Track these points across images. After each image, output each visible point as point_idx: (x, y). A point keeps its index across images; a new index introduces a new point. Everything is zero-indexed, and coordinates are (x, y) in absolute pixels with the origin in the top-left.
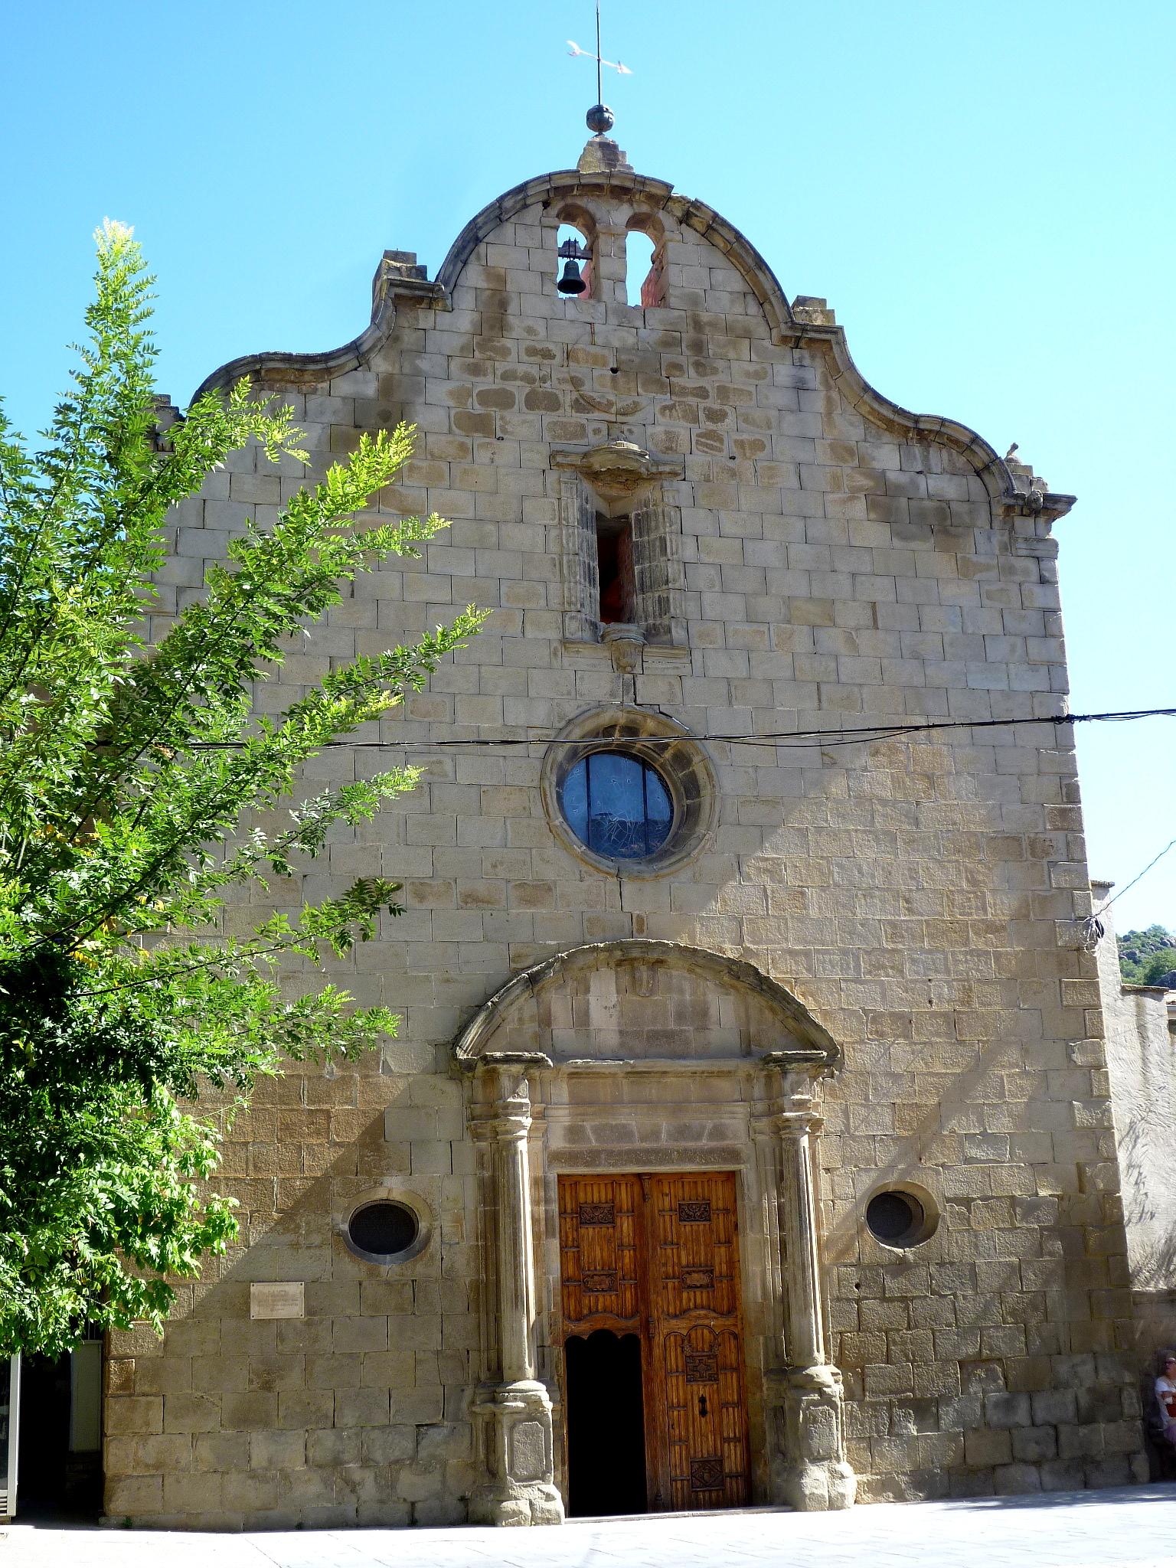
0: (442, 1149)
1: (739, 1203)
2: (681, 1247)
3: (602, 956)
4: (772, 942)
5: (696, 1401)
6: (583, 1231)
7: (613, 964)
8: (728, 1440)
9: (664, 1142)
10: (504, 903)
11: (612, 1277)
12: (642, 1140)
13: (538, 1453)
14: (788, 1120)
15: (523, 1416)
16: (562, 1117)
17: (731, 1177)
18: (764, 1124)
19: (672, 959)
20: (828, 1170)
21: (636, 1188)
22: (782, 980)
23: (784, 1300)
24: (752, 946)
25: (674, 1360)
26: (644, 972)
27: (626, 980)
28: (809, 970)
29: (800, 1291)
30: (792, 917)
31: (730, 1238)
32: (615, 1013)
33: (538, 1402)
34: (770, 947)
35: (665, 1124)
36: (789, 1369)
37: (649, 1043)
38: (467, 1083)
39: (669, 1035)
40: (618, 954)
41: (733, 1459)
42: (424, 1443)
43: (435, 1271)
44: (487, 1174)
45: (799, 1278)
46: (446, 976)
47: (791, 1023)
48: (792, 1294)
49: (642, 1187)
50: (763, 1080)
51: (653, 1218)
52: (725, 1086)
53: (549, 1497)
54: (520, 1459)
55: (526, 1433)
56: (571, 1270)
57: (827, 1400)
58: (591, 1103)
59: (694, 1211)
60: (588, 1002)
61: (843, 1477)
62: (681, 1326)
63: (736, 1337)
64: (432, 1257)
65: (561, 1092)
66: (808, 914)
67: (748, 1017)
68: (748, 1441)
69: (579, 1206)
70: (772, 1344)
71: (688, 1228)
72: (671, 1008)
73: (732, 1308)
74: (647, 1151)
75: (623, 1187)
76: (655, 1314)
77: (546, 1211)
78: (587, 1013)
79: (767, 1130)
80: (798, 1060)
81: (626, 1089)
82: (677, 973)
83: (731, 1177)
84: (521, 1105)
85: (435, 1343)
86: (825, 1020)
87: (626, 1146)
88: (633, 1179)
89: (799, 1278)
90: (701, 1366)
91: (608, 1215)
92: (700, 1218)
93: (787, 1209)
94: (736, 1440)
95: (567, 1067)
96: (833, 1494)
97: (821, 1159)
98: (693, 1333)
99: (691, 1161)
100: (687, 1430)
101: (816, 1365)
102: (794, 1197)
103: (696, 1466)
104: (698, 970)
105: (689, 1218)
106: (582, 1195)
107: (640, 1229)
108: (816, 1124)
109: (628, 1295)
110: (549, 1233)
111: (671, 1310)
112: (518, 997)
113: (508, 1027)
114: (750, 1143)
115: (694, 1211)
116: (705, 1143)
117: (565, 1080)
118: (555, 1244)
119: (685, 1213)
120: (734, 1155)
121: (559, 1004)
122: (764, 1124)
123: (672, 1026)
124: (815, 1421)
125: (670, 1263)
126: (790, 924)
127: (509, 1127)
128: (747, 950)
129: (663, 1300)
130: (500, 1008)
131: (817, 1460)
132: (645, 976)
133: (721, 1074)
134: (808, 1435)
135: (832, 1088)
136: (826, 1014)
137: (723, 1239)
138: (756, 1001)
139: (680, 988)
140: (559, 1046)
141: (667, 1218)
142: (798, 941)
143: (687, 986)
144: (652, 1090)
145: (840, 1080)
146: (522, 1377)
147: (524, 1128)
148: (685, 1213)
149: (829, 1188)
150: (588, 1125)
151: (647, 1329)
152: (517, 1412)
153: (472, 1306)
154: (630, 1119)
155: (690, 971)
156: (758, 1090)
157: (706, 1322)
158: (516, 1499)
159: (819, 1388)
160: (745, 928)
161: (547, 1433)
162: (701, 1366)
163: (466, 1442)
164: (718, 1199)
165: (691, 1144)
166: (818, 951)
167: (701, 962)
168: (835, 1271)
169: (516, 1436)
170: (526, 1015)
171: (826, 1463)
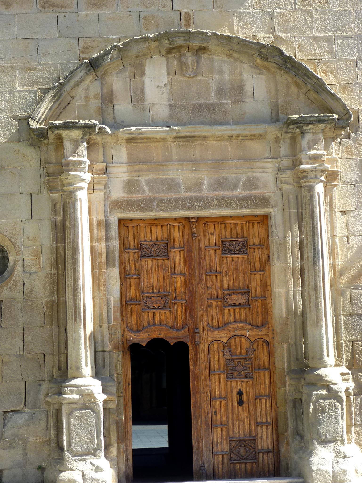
0: (24, 200)
1: (270, 239)
2: (225, 274)
3: (153, 45)
4: (299, 31)
5: (235, 394)
6: (143, 262)
7: (163, 52)
8: (261, 424)
9: (206, 191)
10: (75, 6)
11: (165, 299)
12: (188, 190)
13: (91, 435)
14: (304, 171)
15: (79, 406)
16: (121, 174)
17: (266, 218)
18: (288, 176)
19: (212, 46)
20: (344, 212)
21: (186, 229)
22: (308, 62)
23: (303, 314)
24: (281, 35)
25: (217, 361)
26: (189, 58)
27: (175, 65)
28: (331, 52)
29: (313, 308)
30: (316, 10)
31: (264, 268)
32: (166, 91)
33: (91, 395)
34: (297, 35)
35: (206, 178)
36: (305, 367)
37: (195, 113)
38: (44, 149)
39: (211, 108)
40: (166, 42)
41: (265, 439)
42: (9, 425)
43: (18, 294)
44: (59, 218)
45: (313, 297)
46: (27, 65)
47: (313, 95)
48: (308, 311)
49: (191, 227)
50: (288, 141)
51: (200, 252)
52: (257, 147)
53: (98, 469)
54: (76, 439)
55: (81, 419)
56: (133, 292)
57: (334, 395)
58: (146, 162)
59: (235, 246)
60: (143, 83)
61: (345, 456)
62: (223, 336)
63: (268, 344)
64: (15, 283)
65: (121, 154)
66: (330, 8)
67: (277, 91)
68: (276, 426)
69: (137, 243)
70: (293, 349)
71: (229, 260)
72: (213, 86)
73: (265, 321)
74: (191, 199)
75: (176, 229)
76: (201, 327)
77: (107, 247)
78: (142, 92)
79: (291, 181)
80: (312, 122)
81: (175, 150)
82: (218, 59)
83: (266, 218)
84: (80, 163)
85: (18, 348)
86: (344, 92)
87: (174, 195)
88: (184, 222)
89: (313, 297)
90: (239, 366)
91: (164, 250)
92: (240, 252)
93: (305, 242)
94: (268, 424)
95: (124, 133)
96: (337, 470)
97: (337, 204)
98: (233, 341)
99: (228, 206)
100: (227, 417)
101: (325, 366)
102: (310, 233)
103: (234, 444)
104: (235, 55)
105: (230, 252)
106: (142, 235)
107: (189, 260)
108: (332, 176)
109: (179, 311)
110: (109, 263)
111: (215, 323)
112: (82, 80)
113: (76, 104)
114: (278, 192)
115: (235, 246)
116: (239, 192)
117: (124, 144)
118: (115, 273)
119: (226, 248)
120: (264, 201)
121: (118, 83)
122: (288, 176)
123: (213, 100)
124: (323, 412)
125: (214, 287)
126: (314, 16)
127: (70, 180)
128: (277, 38)
129: (208, 315)
130: (67, 88)
131: (324, 442)
132: (190, 59)
133: (253, 137)
134: (318, 423)
135: (349, 147)
136: (344, 87)
137: (258, 268)
138: (283, 78)
139: (220, 70)
140: (119, 118)
141: (212, 252)
142: (321, 29)
143: (226, 68)
144: (195, 151)
145: (356, 140)
146: (79, 375)
147: (82, 180)
148: (226, 248)
149: (344, 226)
150: (142, 179)
151: (194, 337)
152: (72, 402)
153: (48, 320)
154: (178, 174)
155: (229, 56)
156: (284, 149)
157: (243, 332)
158: (72, 470)
159: (327, 386)
160: (276, 20)
161: (98, 419)
162: (239, 366)
163: (43, 423)
164: (254, 237)
165: (228, 193)
166: (338, 37)
167: (236, 47)
168: (348, 293)
169: (73, 421)
170: (92, 93)
171: (332, 445)
